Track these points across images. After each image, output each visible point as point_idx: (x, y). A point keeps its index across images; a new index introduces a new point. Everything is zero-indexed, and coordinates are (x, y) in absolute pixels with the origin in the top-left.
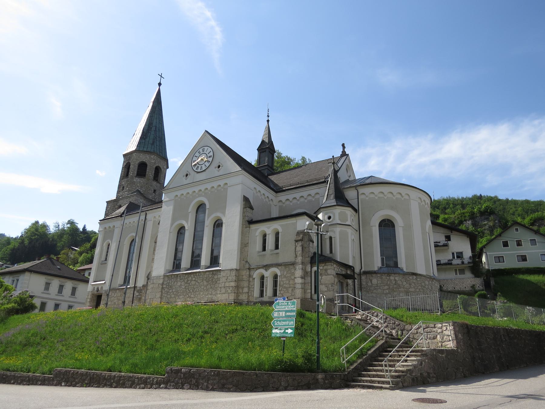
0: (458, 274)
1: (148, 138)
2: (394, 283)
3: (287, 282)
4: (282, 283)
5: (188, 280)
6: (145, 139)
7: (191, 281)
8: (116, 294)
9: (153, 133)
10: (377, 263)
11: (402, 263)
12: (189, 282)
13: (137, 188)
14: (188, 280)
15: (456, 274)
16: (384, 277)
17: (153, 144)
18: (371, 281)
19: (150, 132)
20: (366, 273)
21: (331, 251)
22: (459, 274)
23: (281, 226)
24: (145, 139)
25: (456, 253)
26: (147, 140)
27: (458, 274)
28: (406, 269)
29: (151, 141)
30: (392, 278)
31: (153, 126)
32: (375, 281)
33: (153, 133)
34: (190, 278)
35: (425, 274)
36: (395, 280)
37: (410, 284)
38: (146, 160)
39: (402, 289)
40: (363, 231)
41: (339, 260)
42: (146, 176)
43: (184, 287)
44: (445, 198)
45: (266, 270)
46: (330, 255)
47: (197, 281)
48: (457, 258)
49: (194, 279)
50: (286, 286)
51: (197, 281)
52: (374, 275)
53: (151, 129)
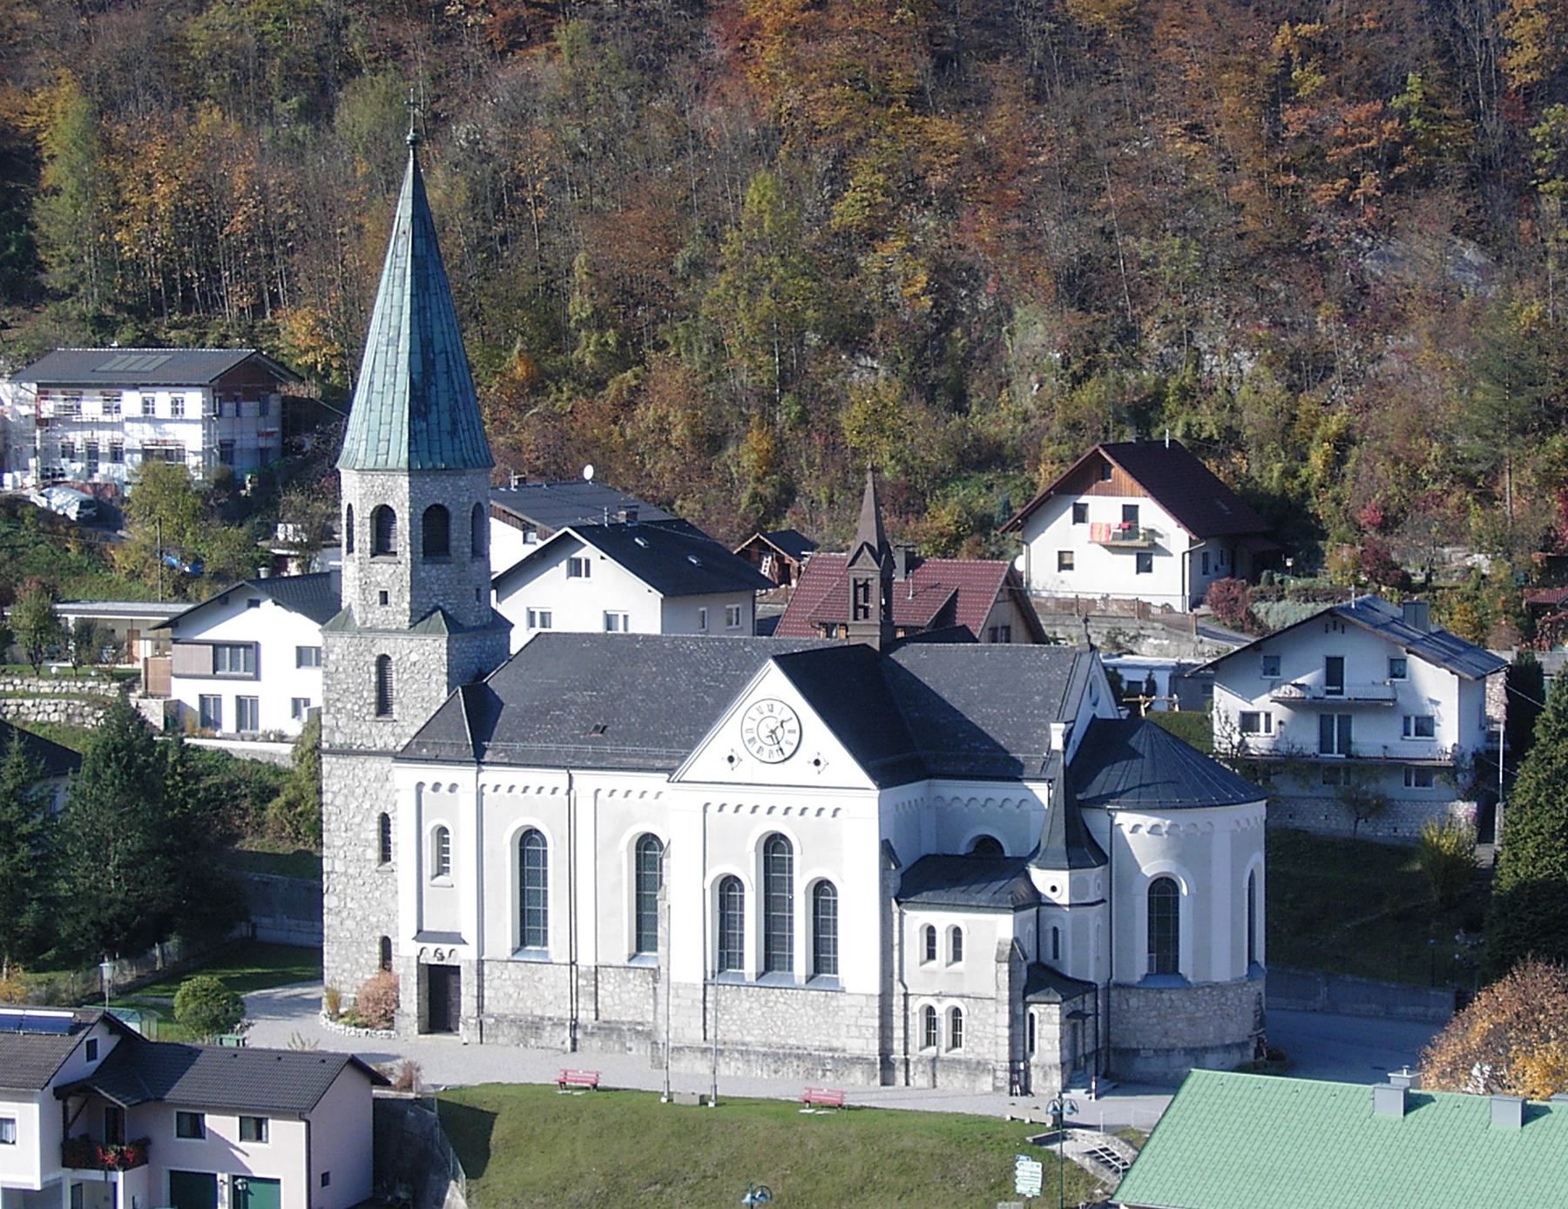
0: (1413, 783)
1: (434, 408)
2: (1168, 1004)
3: (981, 1028)
4: (970, 1029)
5: (767, 1001)
6: (425, 419)
7: (776, 1003)
8: (506, 972)
9: (443, 384)
10: (1139, 963)
11: (1185, 966)
12: (771, 1004)
13: (435, 601)
14: (767, 1001)
15: (1408, 784)
16: (1151, 995)
17: (453, 433)
18: (1127, 1000)
19: (433, 379)
20: (1118, 986)
21: (1056, 956)
22: (1416, 785)
23: (967, 922)
24: (425, 419)
25: (1417, 718)
26: (433, 417)
27: (1413, 783)
28: (1194, 976)
29: (446, 425)
30: (1165, 996)
31: (436, 351)
32: (1133, 1002)
33: (443, 384)
34: (773, 998)
35: (1228, 979)
36: (1171, 999)
37: (1197, 1005)
38: (445, 499)
39: (1183, 1016)
40: (1117, 890)
41: (1070, 975)
42: (452, 551)
43: (759, 1013)
44: (1307, 752)
45: (939, 1001)
46: (1053, 964)
47: (790, 1005)
48: (1417, 735)
49: (782, 1000)
50: (979, 1034)
51: (790, 1005)
52: (1133, 991)
53: (434, 365)
